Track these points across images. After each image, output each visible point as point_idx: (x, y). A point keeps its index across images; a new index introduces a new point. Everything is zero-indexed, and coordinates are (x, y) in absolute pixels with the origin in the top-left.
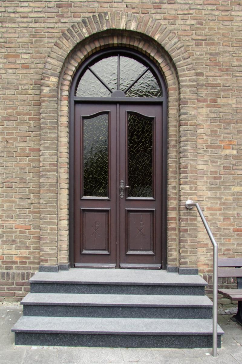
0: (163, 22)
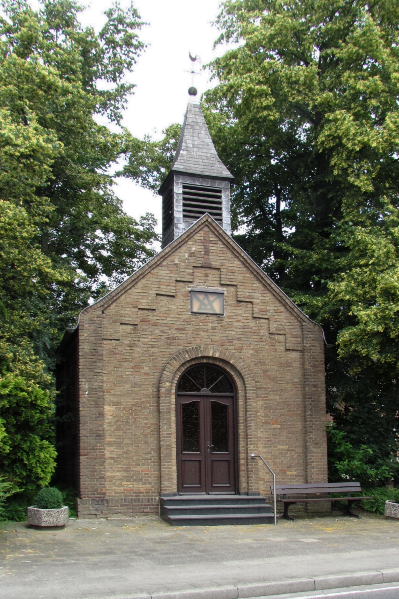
0: (233, 351)
